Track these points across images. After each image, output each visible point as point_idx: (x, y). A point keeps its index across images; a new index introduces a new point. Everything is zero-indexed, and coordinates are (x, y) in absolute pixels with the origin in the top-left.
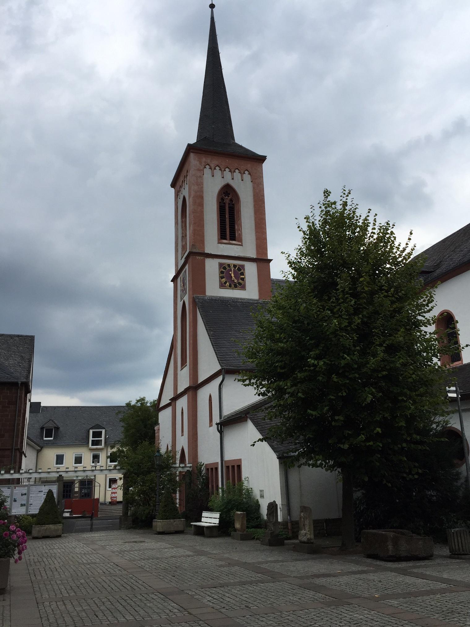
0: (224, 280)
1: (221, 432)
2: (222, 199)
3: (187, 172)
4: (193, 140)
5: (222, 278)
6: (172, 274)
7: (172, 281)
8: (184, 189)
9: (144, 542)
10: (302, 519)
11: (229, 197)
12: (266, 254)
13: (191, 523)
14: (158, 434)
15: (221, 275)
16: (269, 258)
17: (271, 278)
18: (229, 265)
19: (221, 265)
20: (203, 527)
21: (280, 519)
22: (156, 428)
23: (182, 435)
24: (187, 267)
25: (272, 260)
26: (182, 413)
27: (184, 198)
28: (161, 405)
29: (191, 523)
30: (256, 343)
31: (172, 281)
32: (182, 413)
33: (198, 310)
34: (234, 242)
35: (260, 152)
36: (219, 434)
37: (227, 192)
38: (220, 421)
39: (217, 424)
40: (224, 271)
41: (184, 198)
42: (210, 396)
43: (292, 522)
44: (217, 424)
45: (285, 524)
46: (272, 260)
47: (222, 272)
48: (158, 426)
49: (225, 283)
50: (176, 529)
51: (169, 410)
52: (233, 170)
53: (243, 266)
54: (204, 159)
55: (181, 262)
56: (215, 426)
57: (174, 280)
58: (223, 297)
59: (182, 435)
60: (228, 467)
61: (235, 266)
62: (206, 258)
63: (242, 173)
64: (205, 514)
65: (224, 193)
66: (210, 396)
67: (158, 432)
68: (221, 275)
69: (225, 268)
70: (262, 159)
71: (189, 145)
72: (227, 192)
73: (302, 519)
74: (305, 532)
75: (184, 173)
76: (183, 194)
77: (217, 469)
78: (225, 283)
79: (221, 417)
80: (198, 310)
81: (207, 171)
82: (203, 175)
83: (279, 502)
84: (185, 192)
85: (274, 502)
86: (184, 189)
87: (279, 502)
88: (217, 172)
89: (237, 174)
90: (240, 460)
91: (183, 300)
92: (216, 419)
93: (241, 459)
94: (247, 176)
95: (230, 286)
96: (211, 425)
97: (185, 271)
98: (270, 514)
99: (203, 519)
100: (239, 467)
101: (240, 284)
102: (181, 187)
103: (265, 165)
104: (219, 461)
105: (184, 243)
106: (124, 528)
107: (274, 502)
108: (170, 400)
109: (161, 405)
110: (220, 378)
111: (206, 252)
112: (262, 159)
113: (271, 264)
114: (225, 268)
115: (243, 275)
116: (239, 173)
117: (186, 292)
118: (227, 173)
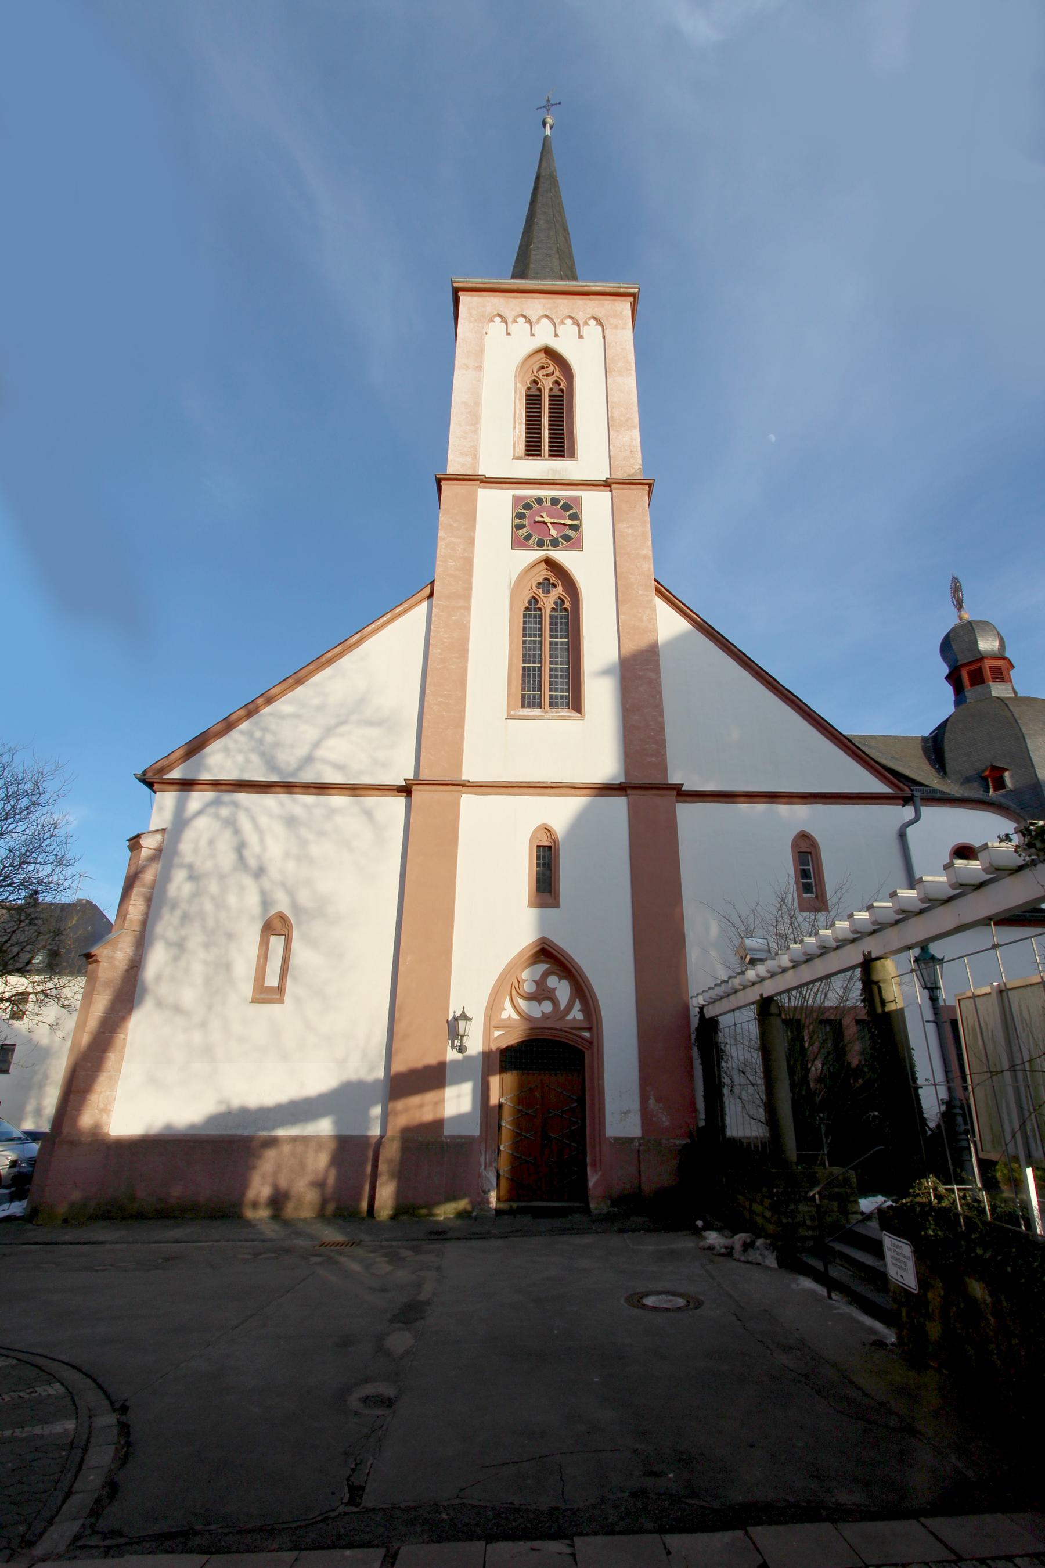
0: (523, 532)
5: (519, 527)
18: (539, 501)
19: (516, 500)
40: (523, 511)
47: (520, 516)
49: (528, 537)
53: (578, 501)
61: (555, 501)
68: (517, 522)
78: (528, 537)
101: (568, 538)
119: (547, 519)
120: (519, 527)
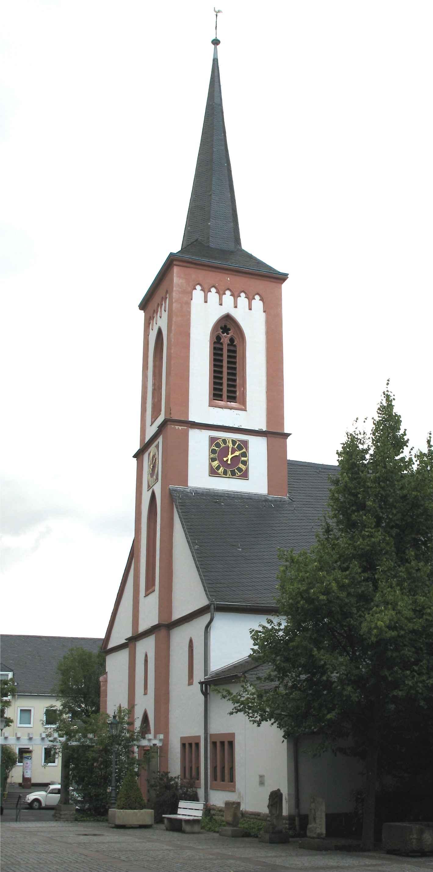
1: (205, 694)
2: (218, 338)
3: (167, 292)
4: (176, 247)
5: (213, 460)
6: (137, 447)
7: (134, 456)
8: (161, 317)
9: (103, 835)
10: (313, 811)
11: (228, 334)
12: (282, 425)
13: (163, 816)
14: (104, 688)
15: (212, 456)
16: (286, 431)
17: (288, 459)
18: (224, 441)
19: (212, 440)
20: (180, 821)
21: (285, 812)
22: (101, 679)
23: (145, 694)
24: (160, 440)
25: (290, 434)
26: (146, 661)
27: (160, 332)
28: (111, 645)
29: (163, 816)
30: (284, 703)
31: (134, 456)
32: (146, 661)
33: (174, 506)
34: (233, 404)
35: (280, 268)
36: (202, 697)
37: (225, 326)
38: (205, 679)
39: (201, 683)
41: (160, 332)
42: (191, 641)
43: (299, 815)
44: (201, 683)
45: (291, 818)
46: (290, 434)
48: (105, 676)
49: (218, 468)
50: (141, 823)
51: (124, 655)
52: (236, 294)
53: (245, 443)
54: (193, 276)
55: (151, 431)
56: (196, 687)
57: (138, 455)
58: (213, 489)
59: (145, 694)
60: (214, 744)
61: (234, 442)
62: (190, 429)
63: (250, 299)
64: (182, 804)
65: (221, 328)
66: (191, 641)
67: (106, 685)
68: (212, 456)
69: (218, 445)
70: (282, 278)
71: (171, 254)
72: (225, 326)
73: (313, 811)
74: (315, 825)
75: (161, 292)
76: (158, 325)
77: (197, 745)
78: (218, 468)
79: (206, 674)
80: (174, 506)
81: (198, 294)
82: (192, 300)
83: (285, 791)
84: (162, 322)
85: (279, 790)
86: (161, 317)
87: (285, 791)
88: (213, 295)
89: (243, 300)
90: (233, 735)
91: (151, 490)
92: (199, 676)
93: (234, 734)
94: (257, 303)
95: (225, 473)
96: (190, 683)
97: (157, 447)
98: (272, 805)
99: (180, 811)
100: (231, 744)
102: (155, 312)
103: (285, 286)
104: (201, 733)
105: (156, 400)
106: (64, 820)
107: (279, 790)
108: (126, 639)
109: (111, 645)
110: (206, 618)
111: (190, 420)
112: (282, 278)
113: (289, 440)
114: (218, 445)
115: (246, 456)
116: (246, 297)
117: (157, 479)
118: (228, 298)
119: (230, 457)
120: (213, 460)
